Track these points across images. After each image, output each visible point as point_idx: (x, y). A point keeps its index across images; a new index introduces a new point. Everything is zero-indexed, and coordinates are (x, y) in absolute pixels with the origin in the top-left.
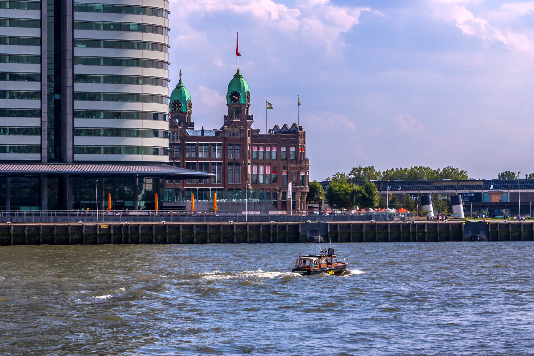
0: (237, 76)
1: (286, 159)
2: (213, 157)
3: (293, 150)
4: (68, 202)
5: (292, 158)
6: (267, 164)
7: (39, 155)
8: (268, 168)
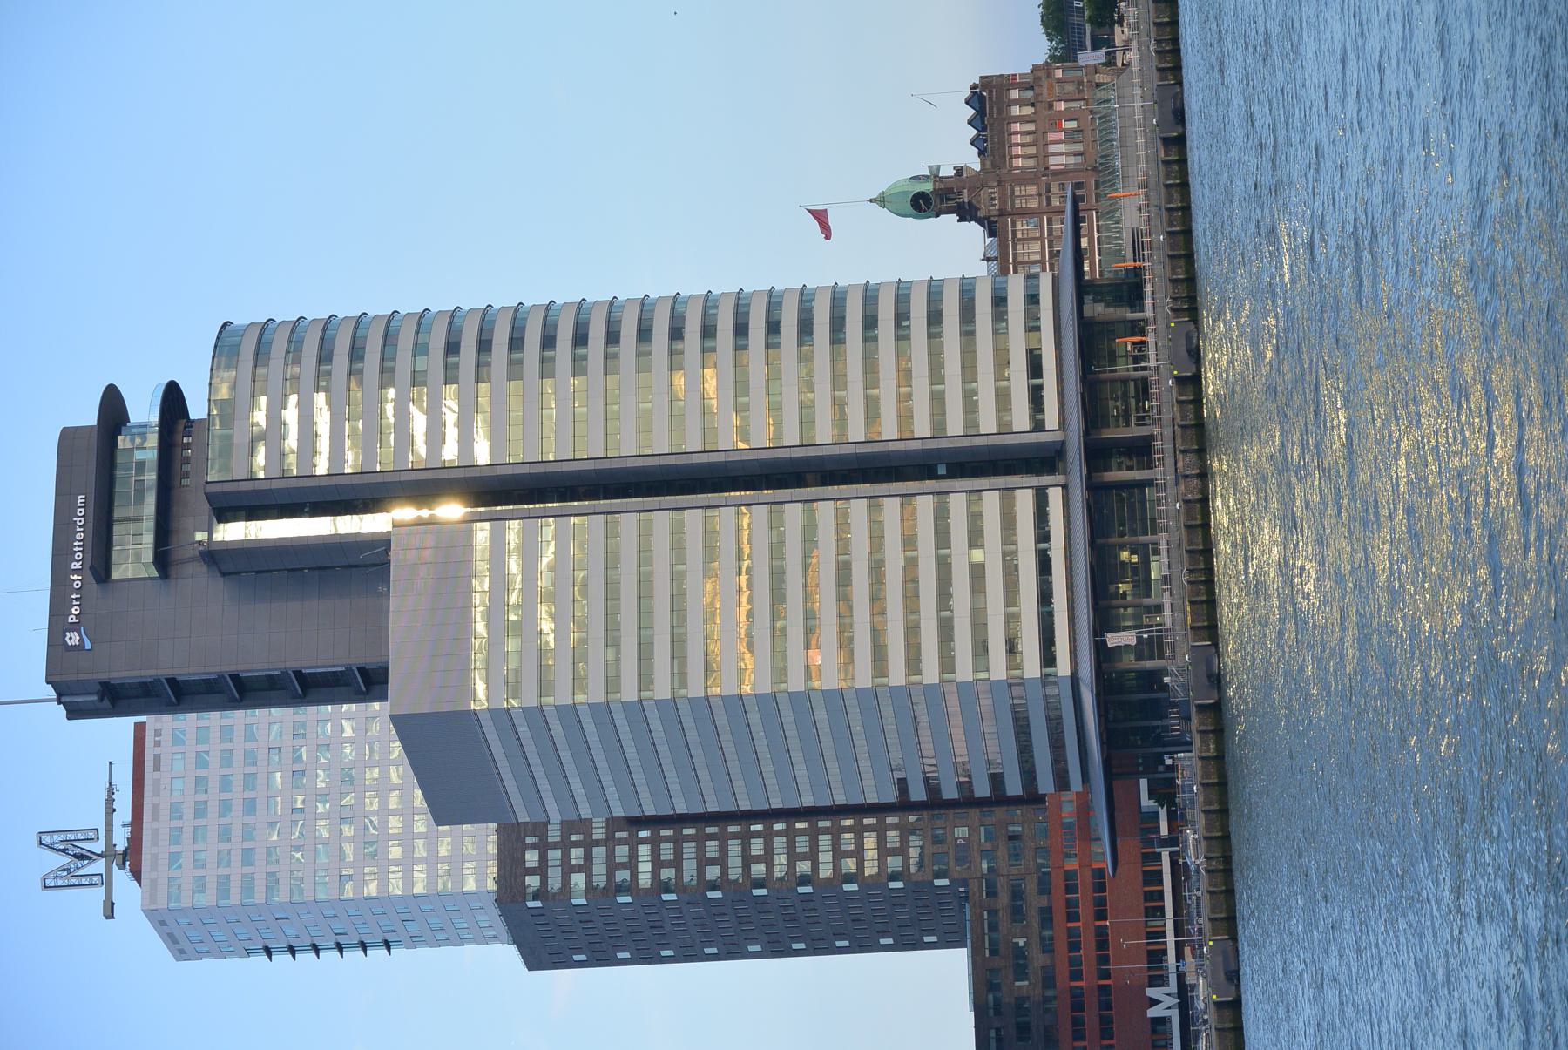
0: (881, 201)
1: (1033, 105)
2: (1038, 257)
3: (1015, 94)
4: (1102, 850)
5: (1030, 94)
6: (1044, 138)
7: (1087, 313)
8: (1052, 137)
